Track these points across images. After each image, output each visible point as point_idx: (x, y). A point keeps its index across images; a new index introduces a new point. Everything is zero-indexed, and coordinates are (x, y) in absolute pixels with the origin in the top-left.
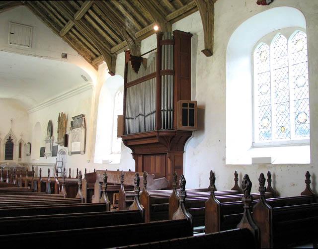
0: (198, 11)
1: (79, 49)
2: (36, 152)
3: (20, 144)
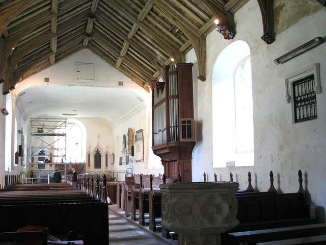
0: (193, 49)
1: (132, 76)
2: (117, 161)
3: (107, 155)
